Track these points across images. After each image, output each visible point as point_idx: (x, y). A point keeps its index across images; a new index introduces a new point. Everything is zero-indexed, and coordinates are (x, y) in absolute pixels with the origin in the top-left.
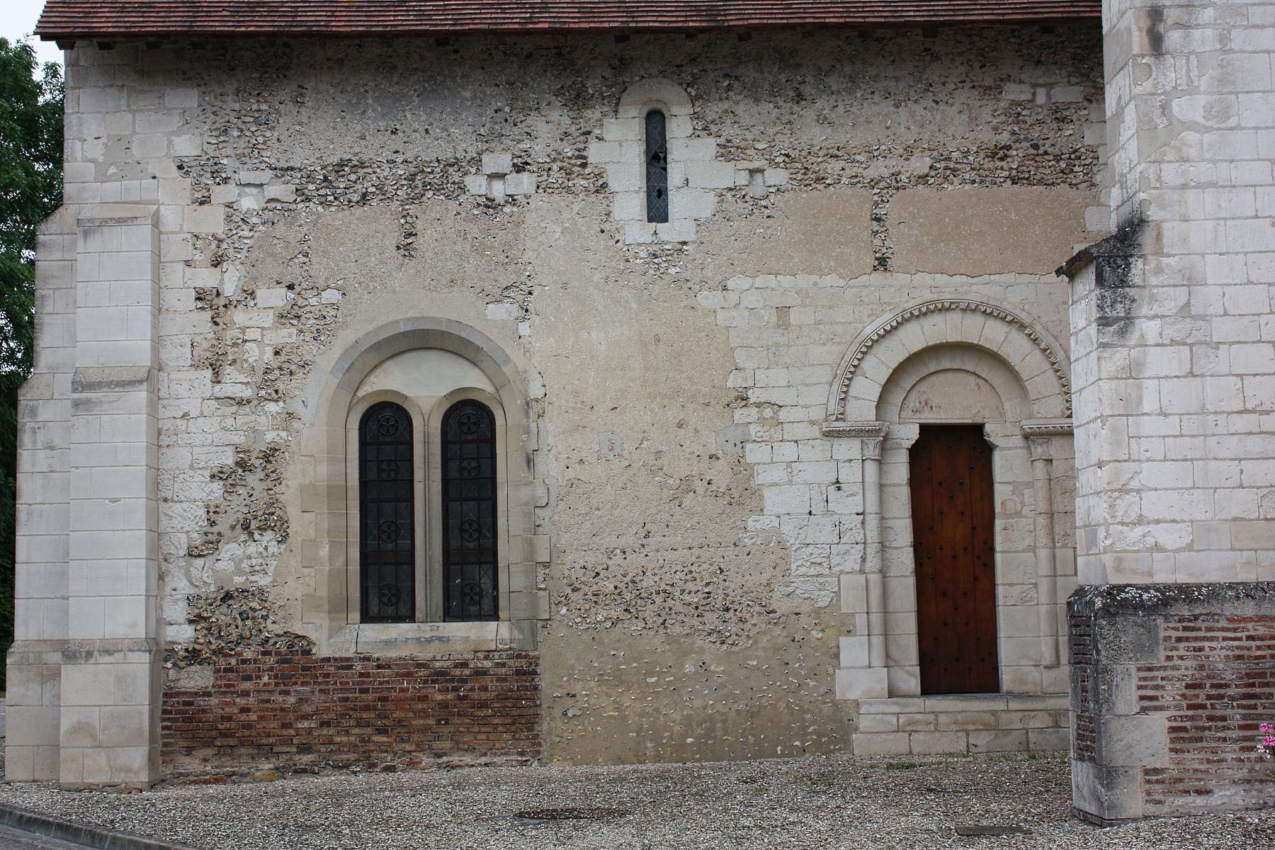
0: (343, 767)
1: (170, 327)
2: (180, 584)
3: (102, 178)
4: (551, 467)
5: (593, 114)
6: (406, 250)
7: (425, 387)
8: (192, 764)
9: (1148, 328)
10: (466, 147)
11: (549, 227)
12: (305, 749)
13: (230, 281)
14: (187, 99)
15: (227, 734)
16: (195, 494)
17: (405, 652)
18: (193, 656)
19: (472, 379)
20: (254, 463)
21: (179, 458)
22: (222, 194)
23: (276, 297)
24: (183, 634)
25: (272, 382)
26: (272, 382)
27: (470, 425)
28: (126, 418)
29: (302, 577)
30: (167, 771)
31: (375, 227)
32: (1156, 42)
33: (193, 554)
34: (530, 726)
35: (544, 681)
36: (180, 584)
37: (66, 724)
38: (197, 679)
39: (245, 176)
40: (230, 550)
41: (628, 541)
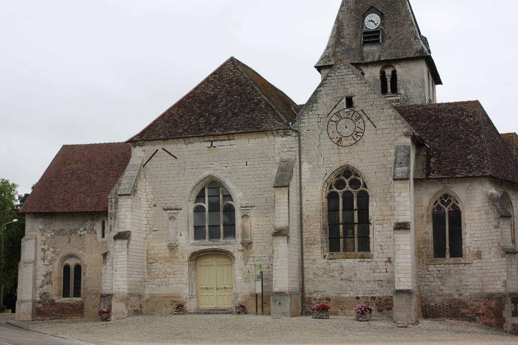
0: (58, 318)
1: (38, 254)
2: (38, 292)
3: (30, 232)
4: (87, 275)
5: (95, 222)
6: (69, 242)
7: (72, 263)
8: (39, 318)
9: (108, 264)
10: (78, 227)
11: (88, 238)
12: (53, 316)
13: (46, 247)
14: (41, 220)
15: (43, 314)
16: (40, 279)
17: (67, 302)
18: (40, 302)
19: (78, 262)
20: (48, 274)
21: (38, 273)
22: (45, 234)
23: (52, 249)
24: (38, 299)
25: (51, 262)
26: (51, 262)
27: (78, 268)
28: (31, 267)
29: (54, 290)
30: (35, 319)
31: (65, 239)
32: (111, 229)
33: (40, 287)
34: (83, 313)
35: (85, 307)
36: (38, 292)
37: (21, 312)
38: (40, 305)
39: (48, 231)
40: (45, 287)
41: (97, 286)
